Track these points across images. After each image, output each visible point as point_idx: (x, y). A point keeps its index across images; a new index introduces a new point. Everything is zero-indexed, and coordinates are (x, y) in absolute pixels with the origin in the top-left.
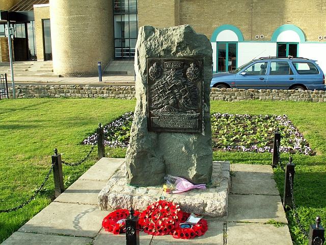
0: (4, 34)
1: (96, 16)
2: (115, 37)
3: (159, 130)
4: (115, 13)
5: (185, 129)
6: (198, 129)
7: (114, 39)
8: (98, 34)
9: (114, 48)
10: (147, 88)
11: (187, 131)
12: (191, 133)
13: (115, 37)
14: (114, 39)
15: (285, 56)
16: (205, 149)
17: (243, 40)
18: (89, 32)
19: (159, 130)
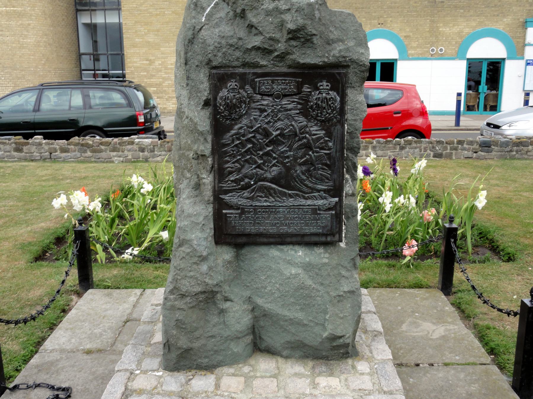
0: (203, 397)
1: (44, 11)
2: (82, 51)
3: (240, 240)
4: (79, 8)
5: (304, 235)
6: (333, 235)
7: (80, 55)
8: (49, 44)
9: (81, 70)
10: (214, 158)
11: (307, 239)
12: (316, 244)
13: (82, 51)
14: (80, 55)
15: (374, 80)
16: (347, 278)
17: (405, 56)
18: (31, 40)
19: (240, 240)
